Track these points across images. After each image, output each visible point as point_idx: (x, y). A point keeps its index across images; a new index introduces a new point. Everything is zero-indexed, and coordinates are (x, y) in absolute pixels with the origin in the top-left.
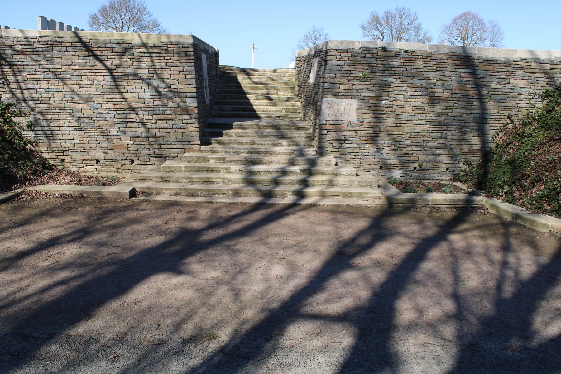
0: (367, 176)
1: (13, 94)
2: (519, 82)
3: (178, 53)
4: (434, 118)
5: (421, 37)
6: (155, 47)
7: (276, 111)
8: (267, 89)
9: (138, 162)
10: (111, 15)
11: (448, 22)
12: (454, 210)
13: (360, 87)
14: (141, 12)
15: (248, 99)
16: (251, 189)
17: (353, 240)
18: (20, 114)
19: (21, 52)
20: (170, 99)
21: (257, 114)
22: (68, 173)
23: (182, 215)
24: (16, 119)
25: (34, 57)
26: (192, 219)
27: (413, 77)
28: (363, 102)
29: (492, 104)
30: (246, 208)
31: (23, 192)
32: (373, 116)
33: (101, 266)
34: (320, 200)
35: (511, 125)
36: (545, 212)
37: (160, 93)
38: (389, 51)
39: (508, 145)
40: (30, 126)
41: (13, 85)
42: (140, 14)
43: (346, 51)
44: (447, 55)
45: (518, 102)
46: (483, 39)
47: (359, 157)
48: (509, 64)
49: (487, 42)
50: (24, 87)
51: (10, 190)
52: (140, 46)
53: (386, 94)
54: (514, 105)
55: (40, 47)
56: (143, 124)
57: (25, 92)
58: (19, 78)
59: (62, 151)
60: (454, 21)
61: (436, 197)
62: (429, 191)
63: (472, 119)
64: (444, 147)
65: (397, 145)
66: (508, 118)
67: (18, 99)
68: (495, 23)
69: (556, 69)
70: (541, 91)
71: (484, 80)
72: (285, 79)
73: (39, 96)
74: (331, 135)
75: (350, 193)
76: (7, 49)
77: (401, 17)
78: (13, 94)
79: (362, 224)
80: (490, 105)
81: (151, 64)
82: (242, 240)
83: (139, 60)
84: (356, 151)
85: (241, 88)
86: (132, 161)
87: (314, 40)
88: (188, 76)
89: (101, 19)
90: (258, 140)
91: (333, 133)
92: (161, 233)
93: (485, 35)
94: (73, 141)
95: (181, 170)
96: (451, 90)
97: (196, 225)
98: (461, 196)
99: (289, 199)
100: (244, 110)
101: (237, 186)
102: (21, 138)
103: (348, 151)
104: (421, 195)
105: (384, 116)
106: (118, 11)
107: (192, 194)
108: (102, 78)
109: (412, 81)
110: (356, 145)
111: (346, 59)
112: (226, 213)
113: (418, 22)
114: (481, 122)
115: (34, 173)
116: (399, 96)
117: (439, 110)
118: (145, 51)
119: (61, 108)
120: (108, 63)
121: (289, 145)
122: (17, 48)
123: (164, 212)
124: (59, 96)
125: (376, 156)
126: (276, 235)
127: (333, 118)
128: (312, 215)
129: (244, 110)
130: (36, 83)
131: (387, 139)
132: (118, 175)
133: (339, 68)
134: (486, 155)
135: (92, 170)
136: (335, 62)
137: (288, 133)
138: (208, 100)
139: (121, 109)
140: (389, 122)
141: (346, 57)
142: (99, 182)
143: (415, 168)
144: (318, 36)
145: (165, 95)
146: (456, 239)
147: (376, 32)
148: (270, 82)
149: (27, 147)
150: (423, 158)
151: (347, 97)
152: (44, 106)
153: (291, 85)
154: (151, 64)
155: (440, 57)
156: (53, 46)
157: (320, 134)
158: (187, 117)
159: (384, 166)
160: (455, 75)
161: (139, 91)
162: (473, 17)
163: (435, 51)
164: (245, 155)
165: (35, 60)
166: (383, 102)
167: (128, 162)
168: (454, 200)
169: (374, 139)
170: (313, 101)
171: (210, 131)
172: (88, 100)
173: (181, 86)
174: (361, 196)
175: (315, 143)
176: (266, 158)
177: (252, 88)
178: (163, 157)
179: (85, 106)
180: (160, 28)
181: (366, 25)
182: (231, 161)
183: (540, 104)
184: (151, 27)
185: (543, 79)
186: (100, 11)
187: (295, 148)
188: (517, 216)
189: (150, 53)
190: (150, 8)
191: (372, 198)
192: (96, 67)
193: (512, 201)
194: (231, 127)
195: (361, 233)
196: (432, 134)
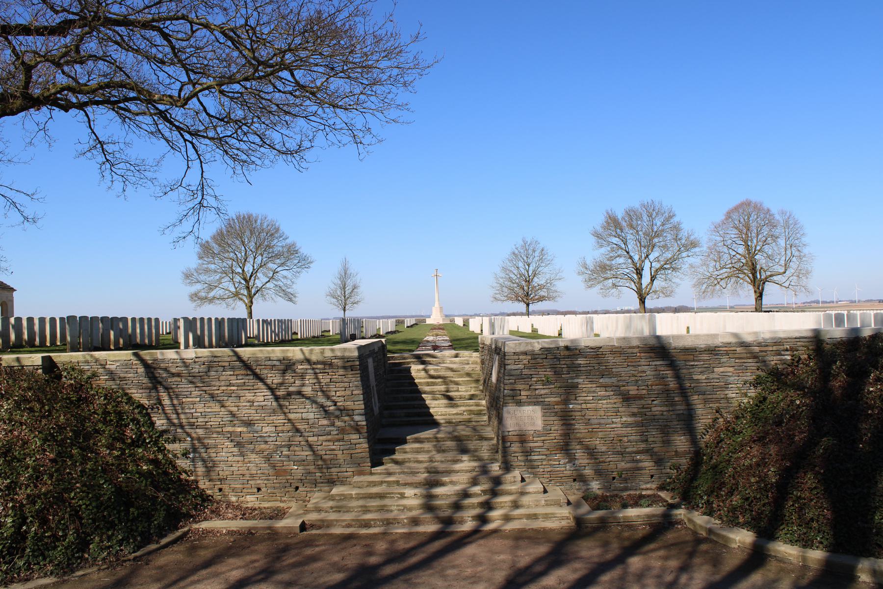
0: (557, 492)
1: (168, 419)
2: (725, 370)
3: (344, 368)
4: (630, 420)
5: (683, 241)
6: (318, 363)
7: (457, 414)
8: (445, 383)
9: (304, 489)
10: (230, 242)
11: (720, 217)
12: (648, 528)
13: (543, 392)
14: (272, 235)
15: (424, 400)
16: (428, 516)
17: (528, 568)
18: (174, 441)
19: (178, 375)
20: (337, 417)
21: (434, 420)
22: (229, 504)
23: (358, 549)
24: (169, 447)
25: (190, 378)
26: (370, 554)
27: (602, 376)
28: (547, 408)
29: (696, 397)
30: (422, 539)
31: (189, 530)
32: (562, 422)
34: (503, 525)
35: (721, 420)
36: (738, 525)
37: (326, 411)
38: (573, 350)
39: (718, 443)
40: (185, 455)
41: (169, 409)
43: (525, 353)
44: (639, 347)
45: (727, 392)
46: (775, 238)
47: (549, 469)
48: (713, 351)
49: (782, 242)
50: (180, 411)
51: (178, 529)
52: (301, 362)
53: (573, 397)
54: (722, 396)
55: (196, 369)
56: (310, 446)
57: (182, 416)
58: (175, 402)
59: (220, 480)
60: (729, 215)
61: (632, 512)
62: (625, 506)
63: (674, 417)
64: (646, 451)
65: (591, 452)
66: (717, 412)
67: (174, 425)
68: (788, 214)
69: (766, 351)
70: (751, 378)
71: (684, 371)
72: (468, 368)
73: (195, 420)
74: (515, 447)
75: (535, 515)
76: (161, 372)
77: (650, 216)
78: (168, 419)
79: (542, 549)
80: (695, 399)
81: (315, 381)
82: (421, 573)
83: (302, 377)
84: (544, 463)
85: (415, 385)
86: (297, 488)
88: (354, 392)
89: (216, 248)
90: (438, 457)
91: (518, 445)
92: (340, 570)
93: (777, 231)
94: (232, 469)
95: (352, 498)
96: (647, 386)
97: (373, 560)
98: (656, 510)
99: (468, 526)
100: (419, 415)
101: (414, 513)
102: (175, 467)
103: (536, 463)
104: (613, 513)
105: (573, 422)
106: (240, 236)
107: (367, 524)
108: (262, 399)
109: (601, 380)
110: (544, 457)
111: (525, 362)
112: (402, 545)
113: (675, 220)
114: (688, 420)
115: (195, 509)
116: (588, 398)
117: (636, 410)
118: (309, 367)
119: (218, 433)
120: (269, 381)
121: (470, 461)
122: (173, 370)
123: (340, 547)
124: (216, 420)
125: (568, 467)
126: (453, 567)
127: (517, 428)
128: (495, 543)
129: (419, 415)
130: (192, 406)
131: (578, 447)
132: (282, 505)
133: (518, 372)
134: (697, 457)
135: (253, 499)
136: (513, 367)
137: (471, 445)
138: (376, 410)
139: (283, 432)
140: (580, 428)
141: (525, 359)
142: (264, 515)
143: (614, 478)
144: (530, 252)
145: (333, 414)
146: (635, 562)
147: (615, 240)
148: (449, 374)
149: (182, 477)
150: (622, 465)
151: (530, 404)
152: (200, 432)
153: (476, 377)
154: (315, 381)
155: (631, 350)
156: (209, 368)
157: (505, 449)
158: (357, 436)
159: (579, 478)
160: (648, 369)
161: (302, 411)
162: (755, 207)
163: (624, 345)
164: (425, 465)
165: (191, 382)
166: (571, 406)
167: (292, 489)
168: (649, 516)
169: (565, 448)
170: (496, 406)
171: (382, 447)
172: (249, 424)
173: (348, 403)
174: (547, 517)
175: (499, 456)
176: (444, 479)
177: (428, 384)
178: (332, 482)
179: (245, 429)
181: (600, 230)
182: (406, 484)
183: (752, 393)
184: (286, 255)
185: (752, 364)
186: (214, 238)
187: (475, 464)
188: (710, 531)
189: (313, 369)
190: (284, 228)
191: (560, 518)
192: (256, 387)
193: (710, 513)
194: (405, 442)
195: (538, 560)
196: (630, 438)
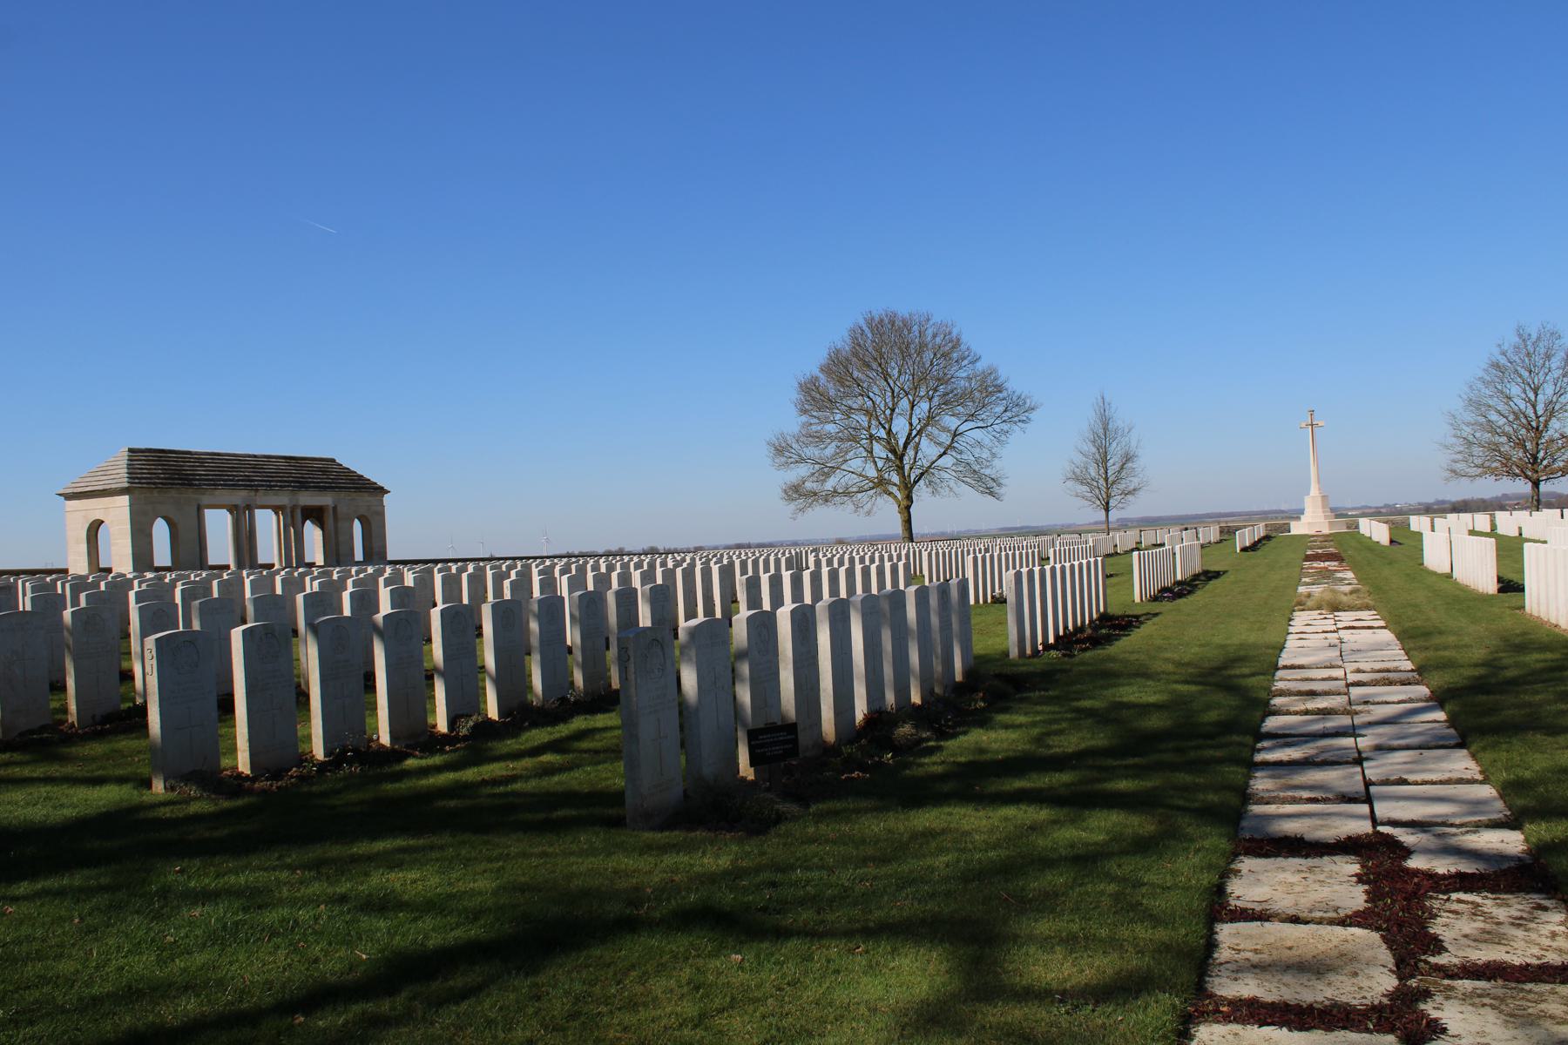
33: (1188, 664)
42: (943, 363)
87: (1525, 374)
180: (1004, 394)
186: (826, 370)
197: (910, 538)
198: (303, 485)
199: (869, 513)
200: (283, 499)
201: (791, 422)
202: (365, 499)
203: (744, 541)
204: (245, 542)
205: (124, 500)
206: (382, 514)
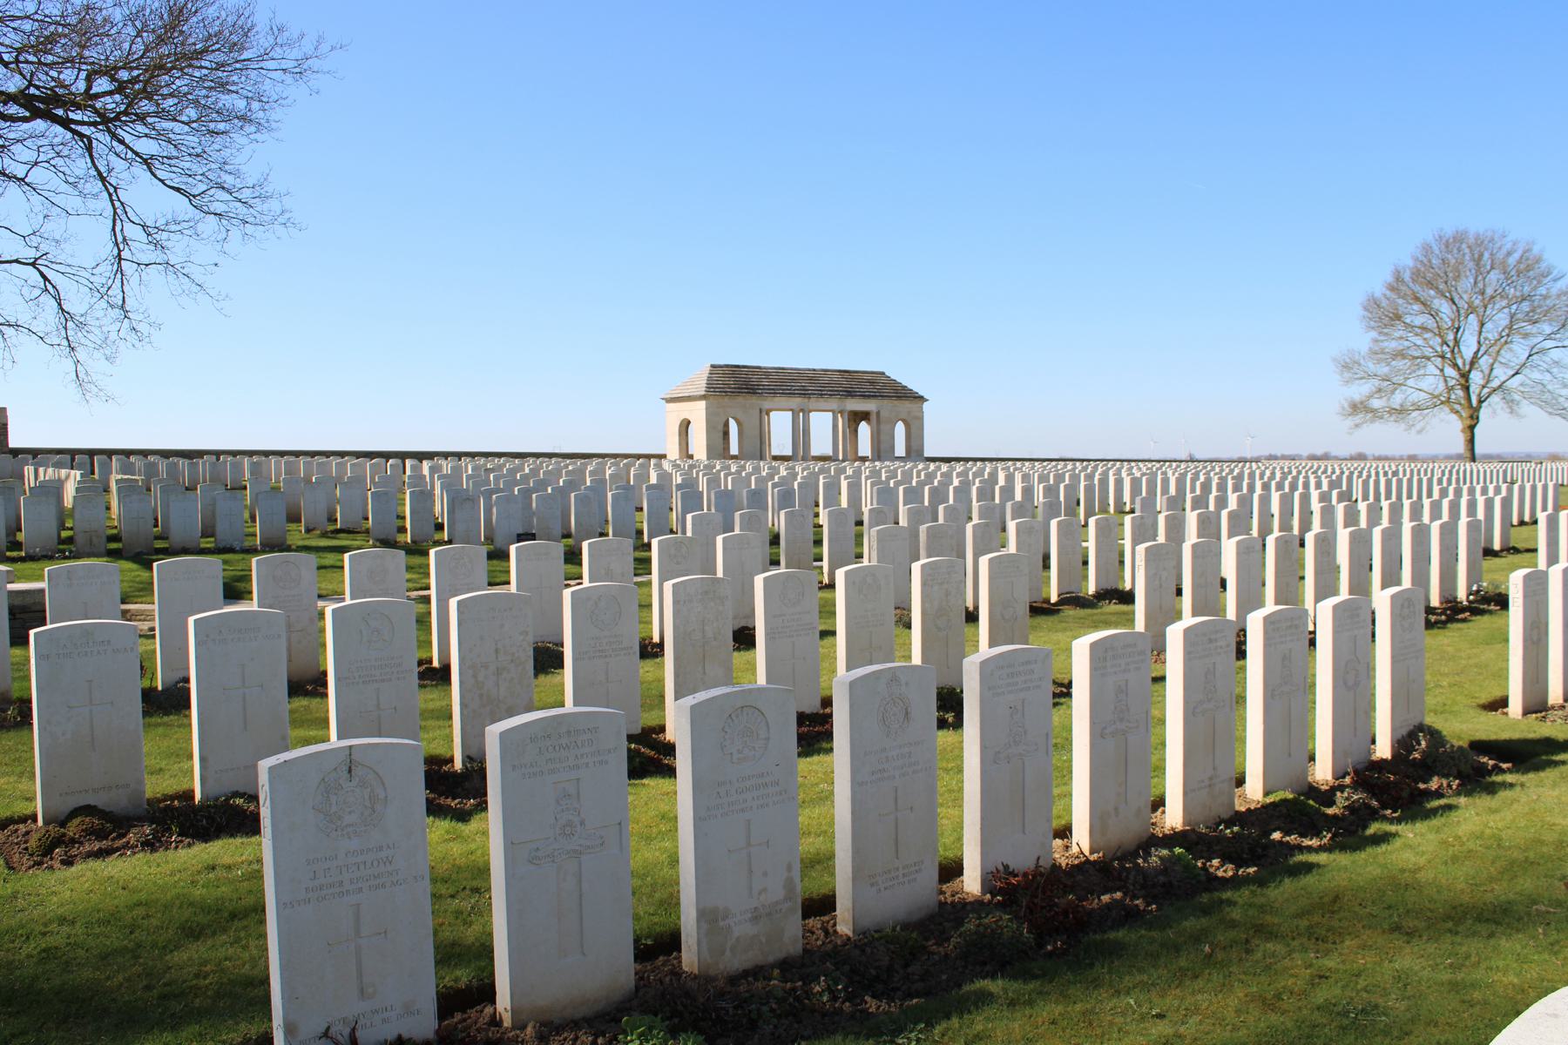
197: (1473, 459)
198: (850, 394)
199: (1419, 432)
200: (834, 403)
201: (1361, 339)
202: (905, 406)
203: (1389, 453)
204: (801, 436)
205: (702, 404)
206: (921, 419)
